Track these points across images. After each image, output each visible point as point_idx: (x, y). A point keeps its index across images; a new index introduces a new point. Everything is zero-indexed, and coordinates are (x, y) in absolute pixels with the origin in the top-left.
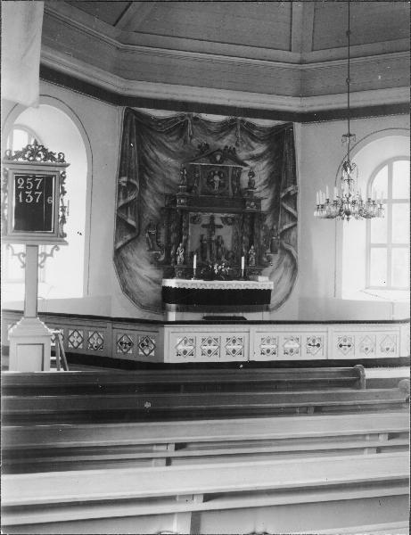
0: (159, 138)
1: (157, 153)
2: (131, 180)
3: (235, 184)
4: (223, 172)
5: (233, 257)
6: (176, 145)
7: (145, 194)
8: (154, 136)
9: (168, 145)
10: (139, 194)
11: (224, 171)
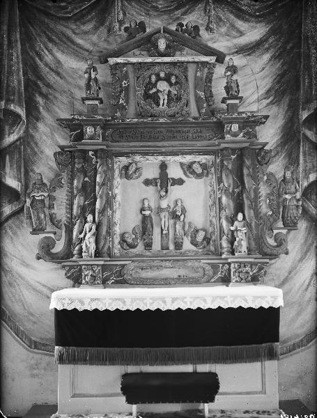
0: (60, 28)
1: (59, 55)
2: (12, 107)
3: (202, 94)
4: (176, 74)
5: (207, 239)
6: (95, 38)
7: (36, 128)
8: (52, 25)
9: (80, 41)
10: (26, 131)
11: (176, 72)
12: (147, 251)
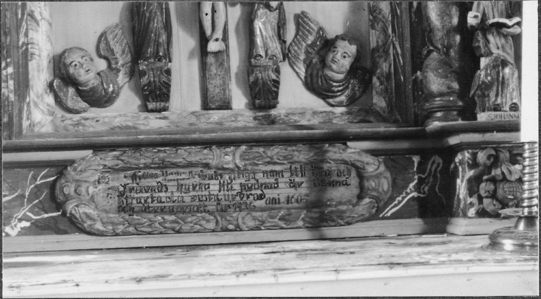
5: (361, 71)
12: (152, 116)
